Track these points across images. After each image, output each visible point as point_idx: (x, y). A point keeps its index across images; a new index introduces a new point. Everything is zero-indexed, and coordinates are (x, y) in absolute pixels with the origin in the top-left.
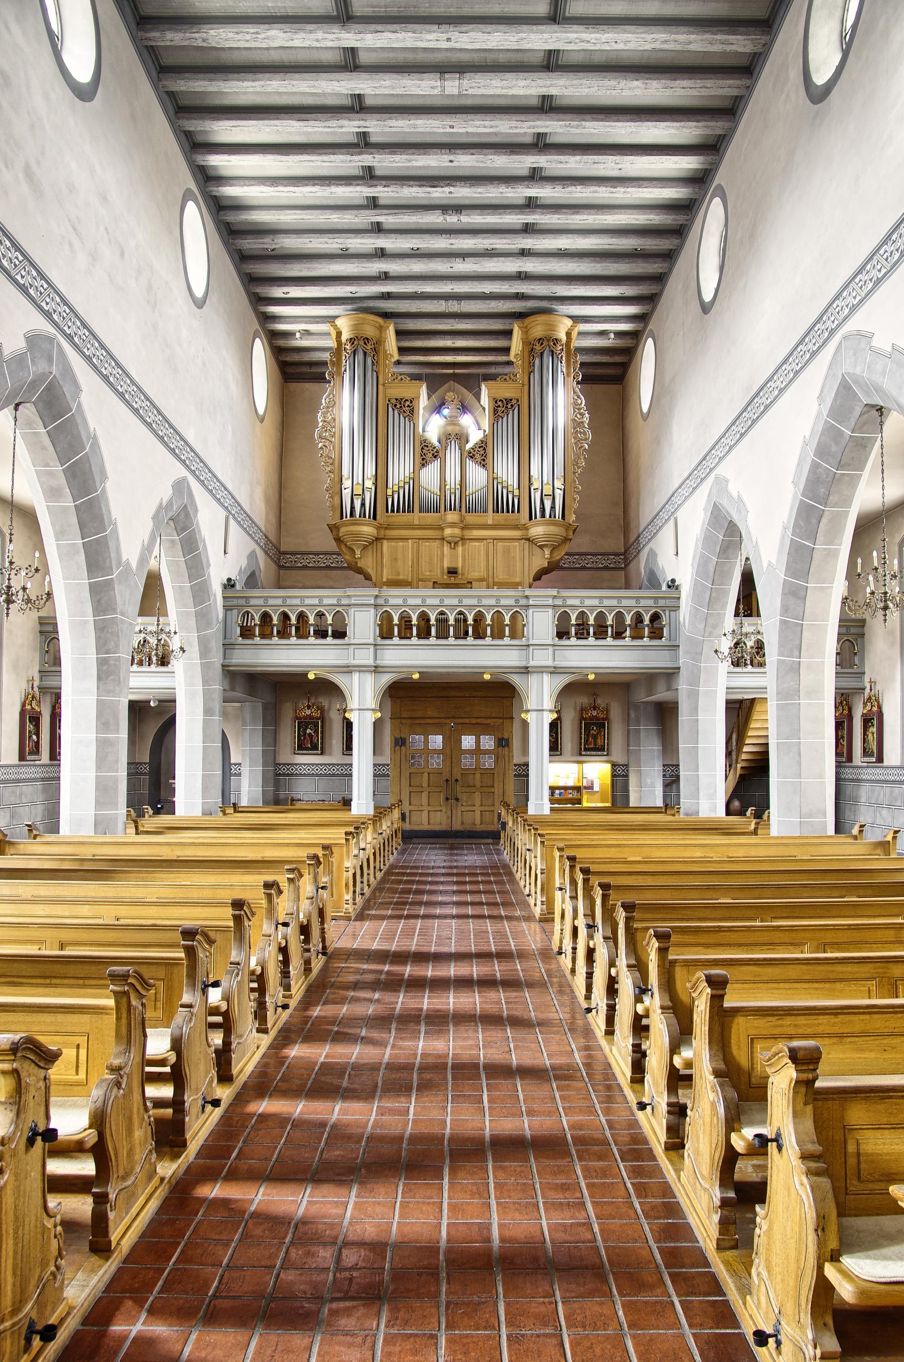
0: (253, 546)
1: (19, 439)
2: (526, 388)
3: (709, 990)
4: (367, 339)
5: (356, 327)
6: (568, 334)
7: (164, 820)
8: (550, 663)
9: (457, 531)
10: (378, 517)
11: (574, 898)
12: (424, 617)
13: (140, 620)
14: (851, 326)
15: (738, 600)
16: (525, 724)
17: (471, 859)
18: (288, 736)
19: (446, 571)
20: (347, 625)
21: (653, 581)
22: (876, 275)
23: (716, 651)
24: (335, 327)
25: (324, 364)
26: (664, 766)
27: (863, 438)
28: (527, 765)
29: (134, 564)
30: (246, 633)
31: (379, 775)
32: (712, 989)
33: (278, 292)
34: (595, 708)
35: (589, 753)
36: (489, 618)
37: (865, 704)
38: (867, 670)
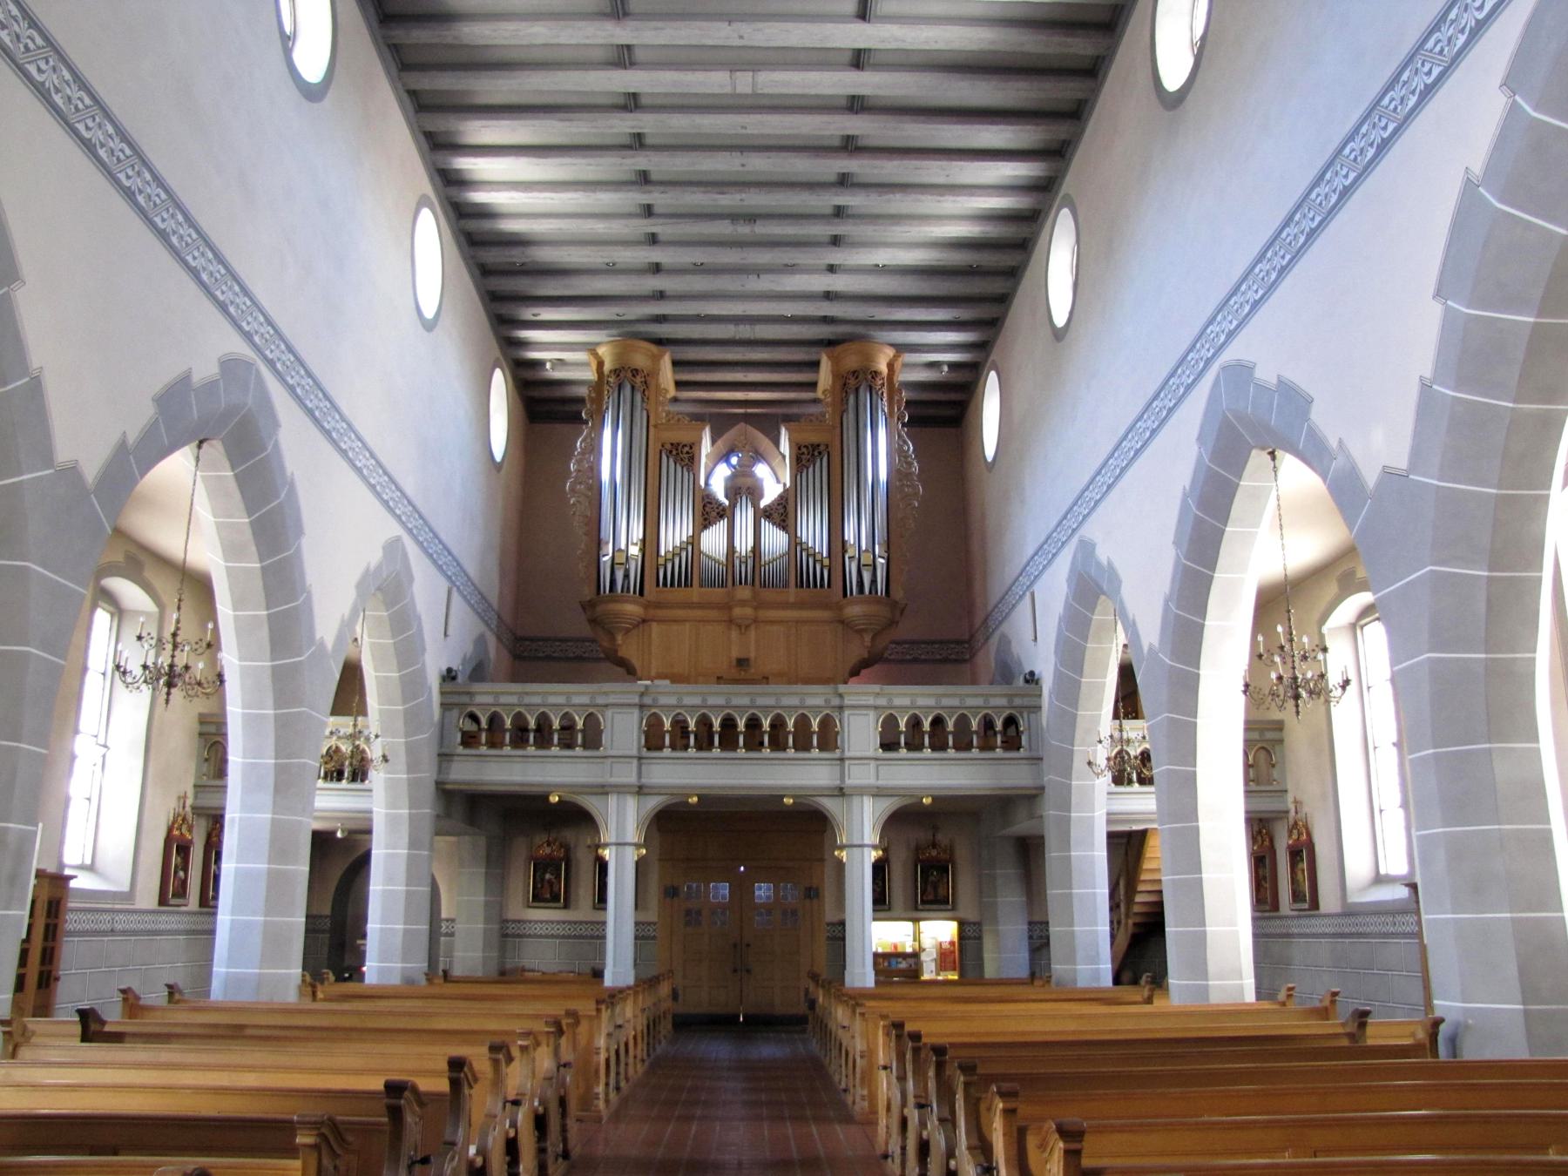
0: (482, 628)
1: (199, 480)
2: (838, 430)
3: (1061, 1145)
4: (636, 370)
5: (620, 356)
6: (890, 366)
7: (351, 987)
8: (872, 781)
9: (748, 611)
10: (646, 592)
11: (902, 1078)
12: (705, 722)
13: (332, 719)
14: (1228, 356)
15: (1116, 702)
16: (840, 865)
17: (768, 1050)
18: (520, 881)
19: (734, 663)
20: (602, 731)
21: (1006, 672)
22: (1340, 183)
23: (1090, 763)
24: (595, 355)
25: (581, 401)
26: (1030, 923)
27: (1254, 487)
28: (842, 924)
29: (329, 645)
30: (469, 740)
31: (643, 938)
32: (1065, 1142)
33: (528, 313)
34: (934, 845)
35: (927, 907)
36: (791, 724)
37: (1290, 833)
38: (1290, 787)
